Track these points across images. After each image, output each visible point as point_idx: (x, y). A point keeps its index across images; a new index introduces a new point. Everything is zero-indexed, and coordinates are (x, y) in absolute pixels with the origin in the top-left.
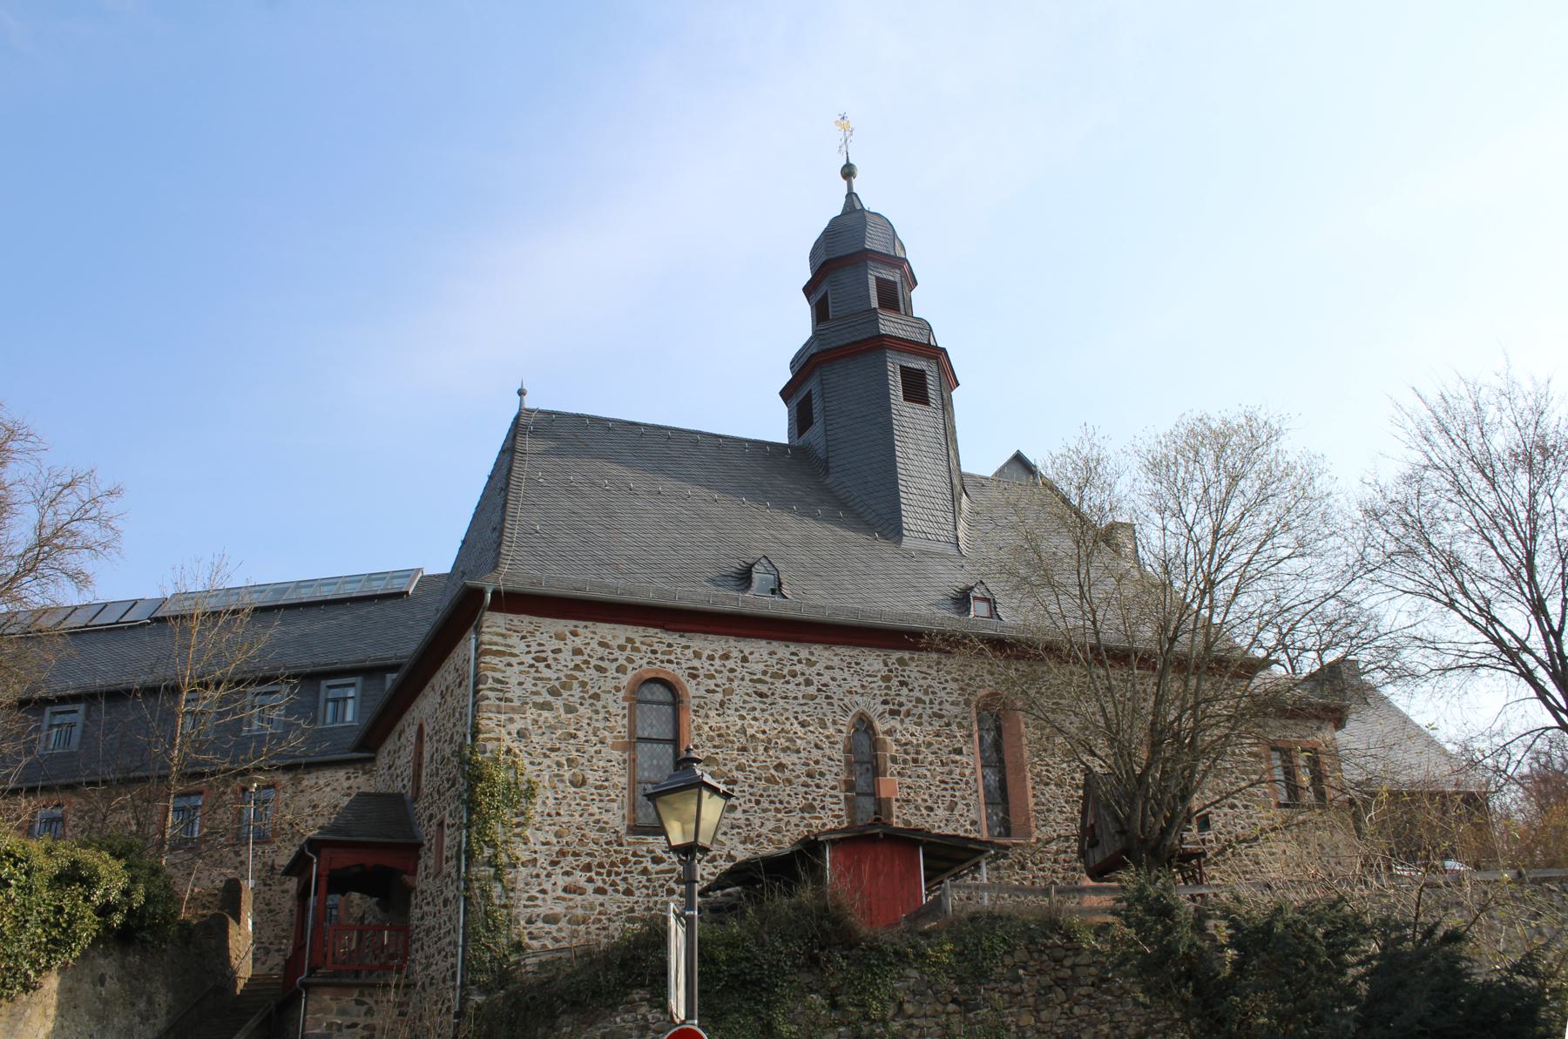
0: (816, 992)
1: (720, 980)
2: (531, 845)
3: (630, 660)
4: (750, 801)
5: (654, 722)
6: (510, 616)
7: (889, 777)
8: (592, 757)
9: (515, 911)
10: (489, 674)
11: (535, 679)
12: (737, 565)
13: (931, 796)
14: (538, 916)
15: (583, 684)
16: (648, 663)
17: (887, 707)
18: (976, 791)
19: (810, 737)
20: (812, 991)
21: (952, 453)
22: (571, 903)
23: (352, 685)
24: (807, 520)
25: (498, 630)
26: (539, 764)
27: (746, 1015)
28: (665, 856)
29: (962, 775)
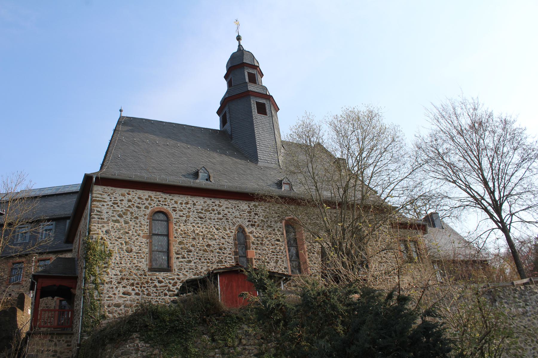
0: (205, 334)
1: (166, 329)
2: (110, 275)
3: (150, 204)
4: (197, 259)
5: (160, 228)
6: (104, 187)
7: (251, 250)
8: (135, 241)
9: (103, 302)
10: (95, 209)
11: (113, 211)
12: (194, 170)
13: (268, 257)
14: (112, 304)
15: (132, 213)
16: (157, 205)
17: (250, 223)
18: (286, 256)
19: (220, 234)
20: (204, 334)
21: (276, 132)
22: (125, 299)
24: (223, 155)
25: (99, 192)
26: (114, 243)
27: (177, 344)
28: (163, 280)
29: (280, 249)
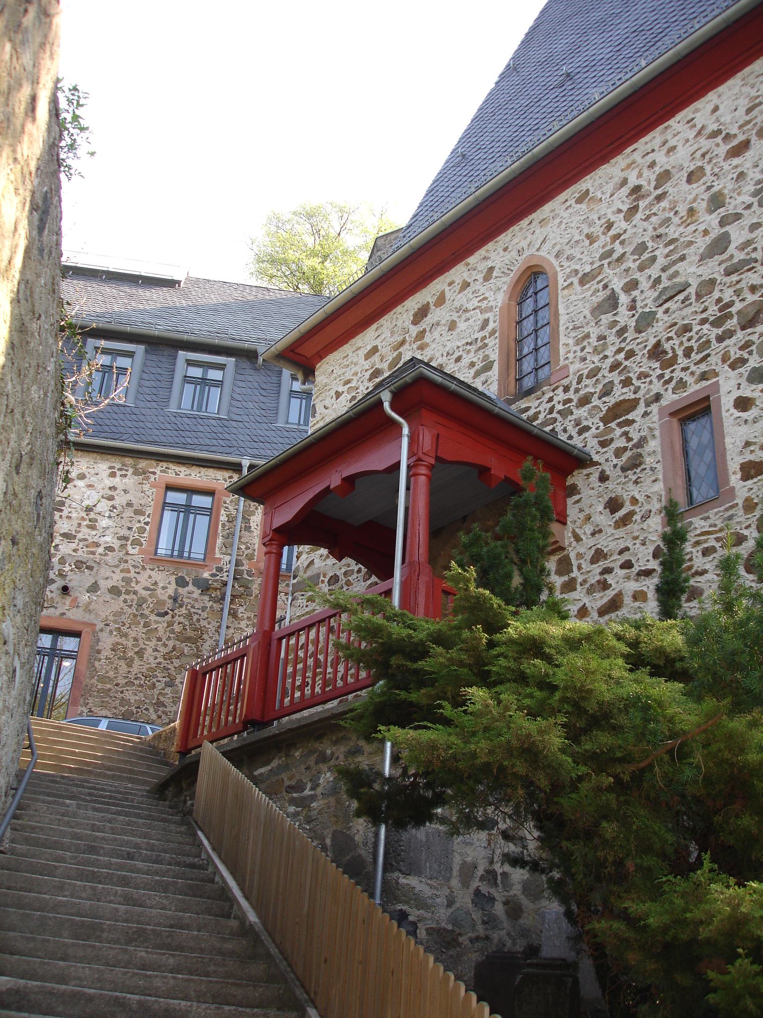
23: (130, 355)
